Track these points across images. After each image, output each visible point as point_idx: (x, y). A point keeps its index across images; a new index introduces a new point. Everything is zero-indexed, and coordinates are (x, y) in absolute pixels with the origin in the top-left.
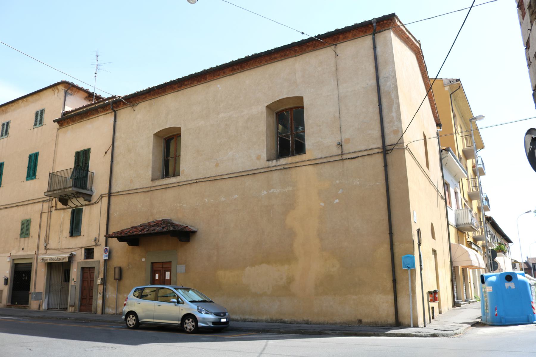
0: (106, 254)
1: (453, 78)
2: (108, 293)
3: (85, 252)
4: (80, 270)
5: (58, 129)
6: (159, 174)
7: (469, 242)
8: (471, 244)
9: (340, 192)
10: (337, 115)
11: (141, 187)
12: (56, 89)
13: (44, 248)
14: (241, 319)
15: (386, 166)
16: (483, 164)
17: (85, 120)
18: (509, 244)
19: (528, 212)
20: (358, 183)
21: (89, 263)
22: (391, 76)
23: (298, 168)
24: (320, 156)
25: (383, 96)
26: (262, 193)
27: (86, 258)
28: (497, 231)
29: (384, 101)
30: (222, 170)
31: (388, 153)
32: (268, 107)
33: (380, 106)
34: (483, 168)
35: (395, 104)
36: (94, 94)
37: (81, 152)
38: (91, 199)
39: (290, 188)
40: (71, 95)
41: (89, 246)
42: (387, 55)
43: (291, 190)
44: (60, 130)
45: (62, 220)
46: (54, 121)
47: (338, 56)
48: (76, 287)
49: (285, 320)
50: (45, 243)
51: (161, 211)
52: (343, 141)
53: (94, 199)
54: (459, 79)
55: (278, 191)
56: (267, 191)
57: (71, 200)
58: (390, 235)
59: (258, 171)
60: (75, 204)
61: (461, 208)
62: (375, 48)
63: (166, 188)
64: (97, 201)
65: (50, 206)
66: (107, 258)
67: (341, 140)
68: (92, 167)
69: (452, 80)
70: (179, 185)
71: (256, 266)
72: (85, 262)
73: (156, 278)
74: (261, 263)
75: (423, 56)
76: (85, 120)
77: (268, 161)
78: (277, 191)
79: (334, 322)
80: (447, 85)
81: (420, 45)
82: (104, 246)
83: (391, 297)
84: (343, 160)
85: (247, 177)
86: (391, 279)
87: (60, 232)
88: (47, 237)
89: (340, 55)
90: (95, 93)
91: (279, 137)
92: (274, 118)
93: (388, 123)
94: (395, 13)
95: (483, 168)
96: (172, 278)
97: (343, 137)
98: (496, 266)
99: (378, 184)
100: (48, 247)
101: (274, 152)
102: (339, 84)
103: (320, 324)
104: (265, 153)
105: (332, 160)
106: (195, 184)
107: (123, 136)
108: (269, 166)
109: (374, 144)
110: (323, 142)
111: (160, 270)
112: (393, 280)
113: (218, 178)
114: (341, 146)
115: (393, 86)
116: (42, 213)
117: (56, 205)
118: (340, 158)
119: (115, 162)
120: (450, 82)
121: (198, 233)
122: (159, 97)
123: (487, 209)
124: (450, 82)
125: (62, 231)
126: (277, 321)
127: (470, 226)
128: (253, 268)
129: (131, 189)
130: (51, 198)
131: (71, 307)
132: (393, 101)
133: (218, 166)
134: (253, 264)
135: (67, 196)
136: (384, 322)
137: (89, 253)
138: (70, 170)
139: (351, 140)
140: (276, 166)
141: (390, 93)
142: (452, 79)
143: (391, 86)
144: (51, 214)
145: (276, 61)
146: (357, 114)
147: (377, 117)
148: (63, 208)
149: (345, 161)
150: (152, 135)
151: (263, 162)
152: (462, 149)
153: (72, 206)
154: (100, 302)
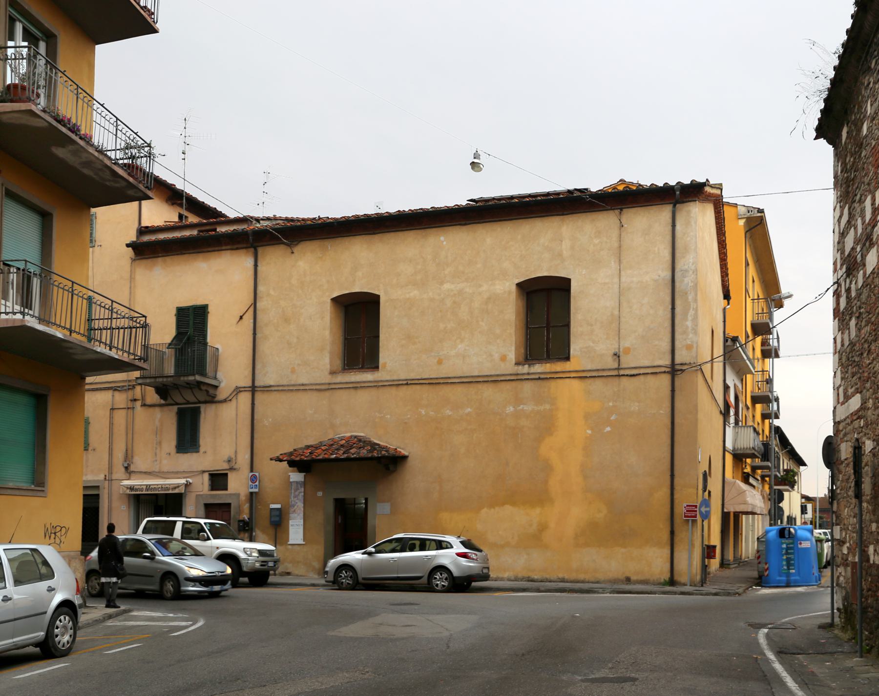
0: (256, 484)
9: (613, 418)
10: (616, 312)
15: (673, 391)
18: (801, 467)
26: (508, 409)
29: (678, 303)
30: (445, 371)
39: (548, 407)
42: (688, 239)
47: (623, 226)
52: (621, 350)
54: (763, 209)
55: (530, 409)
56: (514, 407)
59: (502, 378)
70: (378, 385)
72: (211, 495)
74: (503, 504)
78: (528, 408)
80: (743, 217)
83: (667, 551)
84: (619, 376)
85: (486, 385)
86: (668, 529)
100: (132, 468)
105: (606, 375)
106: (405, 387)
107: (272, 292)
108: (519, 372)
109: (660, 359)
114: (619, 357)
115: (692, 284)
118: (615, 373)
120: (749, 212)
121: (409, 459)
124: (749, 212)
128: (492, 510)
132: (690, 305)
134: (492, 506)
139: (631, 350)
140: (528, 374)
141: (686, 293)
149: (622, 377)
151: (509, 367)
152: (751, 321)
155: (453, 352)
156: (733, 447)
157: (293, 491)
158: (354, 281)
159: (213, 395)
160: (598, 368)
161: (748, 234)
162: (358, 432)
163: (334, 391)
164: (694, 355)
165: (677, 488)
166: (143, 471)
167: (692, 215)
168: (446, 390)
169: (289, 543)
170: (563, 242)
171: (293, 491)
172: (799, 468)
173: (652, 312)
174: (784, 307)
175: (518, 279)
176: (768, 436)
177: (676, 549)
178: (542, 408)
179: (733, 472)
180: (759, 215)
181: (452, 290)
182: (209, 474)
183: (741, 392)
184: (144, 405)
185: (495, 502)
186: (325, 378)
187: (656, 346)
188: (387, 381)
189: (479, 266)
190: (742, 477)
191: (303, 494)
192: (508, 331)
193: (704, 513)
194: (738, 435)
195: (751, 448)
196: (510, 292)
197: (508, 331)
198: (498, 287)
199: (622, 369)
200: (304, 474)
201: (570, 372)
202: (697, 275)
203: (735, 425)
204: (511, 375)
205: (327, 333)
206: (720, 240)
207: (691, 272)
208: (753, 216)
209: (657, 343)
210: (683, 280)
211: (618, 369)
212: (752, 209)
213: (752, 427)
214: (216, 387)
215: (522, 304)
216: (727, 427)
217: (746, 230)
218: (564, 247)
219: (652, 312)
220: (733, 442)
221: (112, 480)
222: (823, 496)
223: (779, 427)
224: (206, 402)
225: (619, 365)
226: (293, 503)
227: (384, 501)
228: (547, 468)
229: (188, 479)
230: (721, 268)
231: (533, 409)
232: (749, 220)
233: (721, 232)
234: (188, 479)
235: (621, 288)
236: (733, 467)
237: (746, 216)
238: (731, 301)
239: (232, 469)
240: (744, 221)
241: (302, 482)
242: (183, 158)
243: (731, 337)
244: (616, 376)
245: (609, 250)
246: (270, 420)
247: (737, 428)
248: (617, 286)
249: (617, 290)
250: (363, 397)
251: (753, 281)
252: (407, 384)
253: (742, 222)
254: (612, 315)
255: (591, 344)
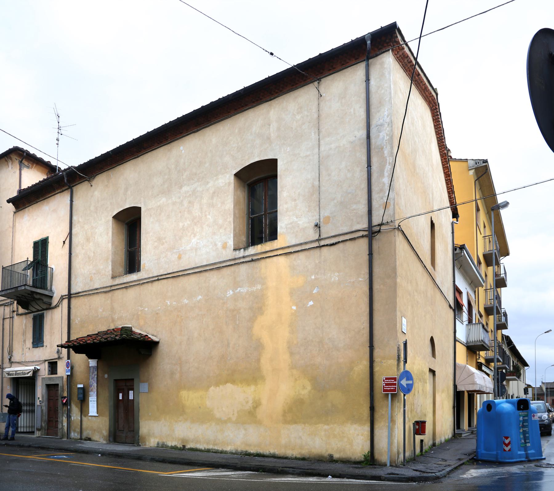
0: (69, 369)
1: (480, 159)
2: (73, 415)
3: (49, 367)
4: (45, 387)
5: (15, 213)
6: (121, 269)
7: (480, 363)
8: (482, 366)
9: (315, 291)
10: (317, 183)
11: (102, 286)
12: (9, 159)
13: (8, 360)
14: (205, 449)
15: (371, 254)
16: (505, 273)
17: (41, 199)
18: (525, 367)
19: (548, 332)
20: (337, 278)
21: (54, 379)
22: (385, 123)
23: (268, 260)
24: (293, 243)
25: (373, 153)
26: (228, 293)
27: (50, 373)
28: (513, 353)
29: (374, 160)
30: (185, 264)
31: (374, 236)
32: (236, 175)
33: (369, 167)
34: (505, 278)
35: (388, 164)
36: (56, 168)
37: (39, 242)
38: (51, 301)
39: (259, 287)
40: (28, 167)
41: (52, 360)
42: (383, 91)
43: (259, 288)
44: (17, 213)
45: (24, 327)
46: (8, 201)
47: (321, 96)
48: (41, 407)
49: (250, 452)
50: (9, 355)
51: (122, 316)
52: (322, 220)
53: (55, 301)
54: (487, 160)
55: (245, 290)
56: (233, 291)
57: (36, 302)
58: (370, 349)
59: (224, 264)
60: (41, 307)
61: (474, 322)
62: (368, 80)
63: (127, 286)
64: (57, 305)
65: (12, 311)
66: (69, 374)
67: (320, 219)
68: (51, 262)
69: (479, 161)
70: (140, 283)
71: (221, 386)
72: (49, 378)
73: (120, 399)
74: (226, 382)
75: (440, 114)
76: (41, 199)
77: (234, 251)
78: (243, 290)
79: (303, 457)
80: (472, 168)
81: (437, 94)
82: (67, 359)
83: (367, 428)
84: (320, 247)
85: (212, 273)
86: (368, 405)
87: (23, 342)
88: (11, 348)
89: (324, 95)
90: (59, 167)
91: (251, 218)
92: (245, 192)
93: (378, 193)
94: (396, 22)
95: (505, 278)
96: (134, 399)
97: (321, 215)
98: (504, 390)
99: (360, 279)
100: (12, 360)
101: (244, 239)
102: (321, 138)
103: (286, 458)
104: (232, 239)
105: (307, 248)
106: (157, 282)
107: (80, 220)
108: (236, 257)
109: (358, 223)
110: (299, 223)
111: (123, 389)
112: (370, 407)
113: (180, 274)
114: (320, 227)
115: (388, 137)
116: (4, 319)
117: (17, 308)
118: (316, 245)
119: (73, 255)
120: (476, 164)
121: (160, 344)
122: (117, 166)
123: (504, 326)
124: (476, 164)
125: (25, 341)
126: (242, 452)
127: (481, 344)
128: (218, 388)
129: (91, 288)
130: (12, 300)
131: (38, 431)
132: (386, 160)
133: (181, 258)
134: (217, 384)
135: (23, 297)
136: (358, 459)
137: (53, 366)
138: (22, 263)
139: (331, 219)
140: (244, 257)
141: (382, 148)
142: (479, 160)
143: (385, 138)
144: (13, 319)
145: (247, 108)
146: (341, 182)
147: (364, 185)
148: (24, 312)
149: (323, 248)
150: (111, 219)
151: (229, 254)
152: (483, 253)
153: (33, 311)
154: (65, 424)
155: (188, 248)
156: (466, 341)
157: (91, 374)
158: (126, 199)
159: (49, 304)
160: (302, 242)
161: (477, 182)
162: (128, 324)
163: (114, 291)
164: (392, 213)
165: (377, 359)
166: (17, 361)
167: (386, 66)
168: (183, 281)
169: (89, 415)
170: (271, 126)
171: (91, 374)
172: (524, 368)
173: (349, 175)
174: (510, 255)
175: (235, 169)
176: (493, 330)
177: (376, 426)
178: (254, 289)
179: (467, 361)
180: (484, 164)
181: (188, 192)
182: (48, 362)
183: (474, 302)
184: (17, 315)
185: (219, 381)
186: (109, 282)
187: (354, 210)
188: (145, 279)
189: (207, 165)
190: (476, 366)
191: (96, 376)
192: (228, 220)
193: (405, 386)
194: (470, 331)
195: (481, 340)
196: (229, 184)
197: (228, 220)
198: (220, 181)
199: (322, 239)
200: (97, 360)
201: (277, 249)
202: (392, 126)
203: (469, 323)
204: (230, 260)
205: (110, 245)
206: (441, 152)
207: (386, 126)
208: (479, 166)
209: (354, 206)
210: (379, 136)
211: (318, 240)
212: (479, 161)
213: (481, 324)
214: (51, 297)
215: (242, 195)
216: (457, 322)
217: (476, 179)
218: (271, 130)
219: (349, 175)
220: (466, 336)
221: (3, 368)
222: (539, 386)
223: (508, 336)
224: (47, 309)
225: (320, 235)
226: (91, 383)
227: (144, 382)
228: (259, 347)
229: (36, 366)
230: (447, 184)
231: (248, 290)
232: (477, 170)
233: (442, 144)
234: (36, 366)
235: (321, 158)
236: (467, 356)
237: (474, 167)
238: (459, 219)
239: (59, 358)
240: (473, 171)
241: (96, 366)
242: (57, 143)
243: (459, 246)
244: (317, 247)
245: (309, 122)
246: (79, 319)
247: (469, 326)
248: (316, 156)
249: (316, 161)
250: (132, 293)
251: (485, 227)
252: (158, 280)
253: (472, 172)
254: (313, 186)
255: (295, 219)
